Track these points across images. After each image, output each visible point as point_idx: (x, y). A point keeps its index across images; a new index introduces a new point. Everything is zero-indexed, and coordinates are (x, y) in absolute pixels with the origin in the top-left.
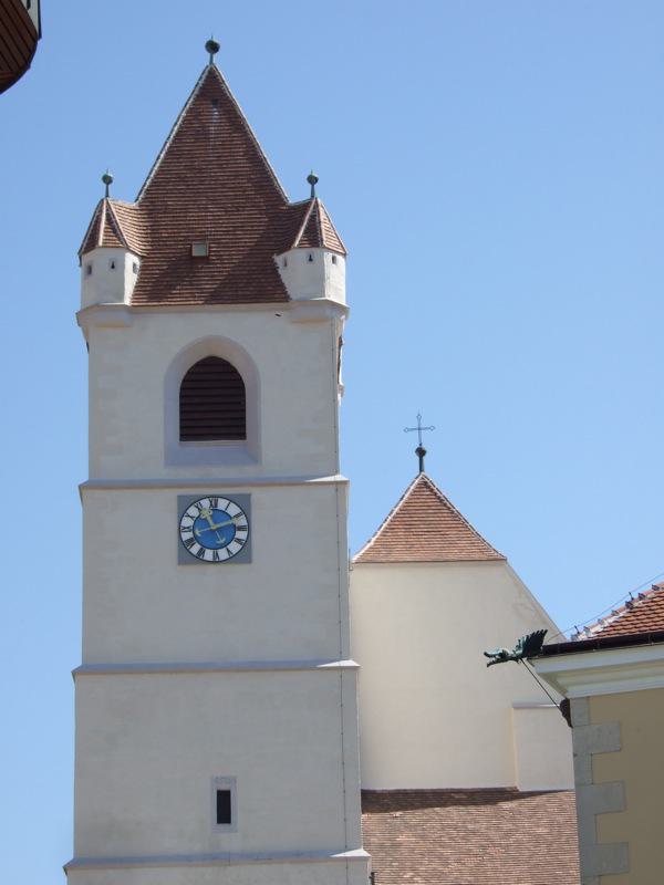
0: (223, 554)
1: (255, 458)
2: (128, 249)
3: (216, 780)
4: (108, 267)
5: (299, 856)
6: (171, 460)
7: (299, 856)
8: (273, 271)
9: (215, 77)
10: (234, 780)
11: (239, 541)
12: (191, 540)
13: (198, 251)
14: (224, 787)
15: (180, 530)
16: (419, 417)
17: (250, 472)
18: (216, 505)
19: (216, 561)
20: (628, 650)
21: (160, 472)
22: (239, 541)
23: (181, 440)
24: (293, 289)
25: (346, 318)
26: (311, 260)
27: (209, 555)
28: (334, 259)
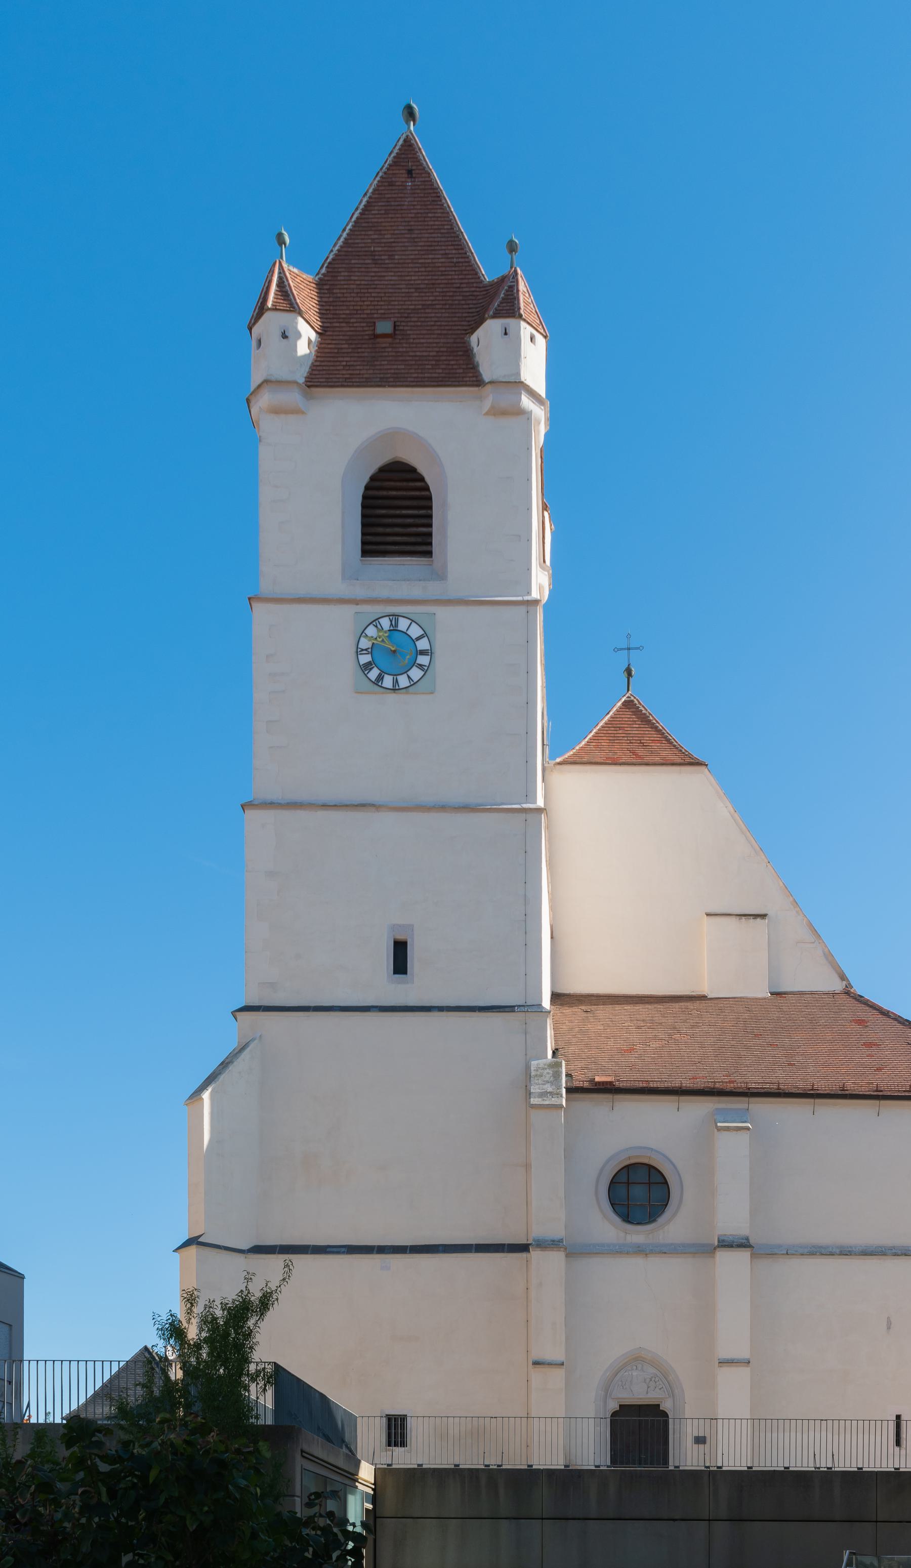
0: (403, 681)
1: (441, 576)
2: (300, 313)
3: (393, 927)
4: (278, 334)
5: (756, 916)
6: (349, 575)
7: (756, 916)
8: (467, 354)
9: (411, 145)
10: (411, 927)
11: (421, 666)
12: (369, 663)
13: (383, 327)
14: (401, 937)
15: (359, 651)
16: (629, 636)
17: (433, 589)
18: (397, 625)
19: (395, 689)
20: (606, 993)
21: (339, 588)
22: (421, 666)
23: (362, 556)
24: (487, 373)
25: (515, 254)
26: (506, 334)
27: (388, 681)
28: (532, 339)
